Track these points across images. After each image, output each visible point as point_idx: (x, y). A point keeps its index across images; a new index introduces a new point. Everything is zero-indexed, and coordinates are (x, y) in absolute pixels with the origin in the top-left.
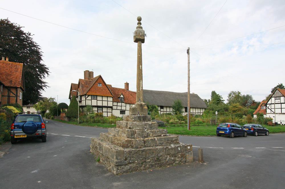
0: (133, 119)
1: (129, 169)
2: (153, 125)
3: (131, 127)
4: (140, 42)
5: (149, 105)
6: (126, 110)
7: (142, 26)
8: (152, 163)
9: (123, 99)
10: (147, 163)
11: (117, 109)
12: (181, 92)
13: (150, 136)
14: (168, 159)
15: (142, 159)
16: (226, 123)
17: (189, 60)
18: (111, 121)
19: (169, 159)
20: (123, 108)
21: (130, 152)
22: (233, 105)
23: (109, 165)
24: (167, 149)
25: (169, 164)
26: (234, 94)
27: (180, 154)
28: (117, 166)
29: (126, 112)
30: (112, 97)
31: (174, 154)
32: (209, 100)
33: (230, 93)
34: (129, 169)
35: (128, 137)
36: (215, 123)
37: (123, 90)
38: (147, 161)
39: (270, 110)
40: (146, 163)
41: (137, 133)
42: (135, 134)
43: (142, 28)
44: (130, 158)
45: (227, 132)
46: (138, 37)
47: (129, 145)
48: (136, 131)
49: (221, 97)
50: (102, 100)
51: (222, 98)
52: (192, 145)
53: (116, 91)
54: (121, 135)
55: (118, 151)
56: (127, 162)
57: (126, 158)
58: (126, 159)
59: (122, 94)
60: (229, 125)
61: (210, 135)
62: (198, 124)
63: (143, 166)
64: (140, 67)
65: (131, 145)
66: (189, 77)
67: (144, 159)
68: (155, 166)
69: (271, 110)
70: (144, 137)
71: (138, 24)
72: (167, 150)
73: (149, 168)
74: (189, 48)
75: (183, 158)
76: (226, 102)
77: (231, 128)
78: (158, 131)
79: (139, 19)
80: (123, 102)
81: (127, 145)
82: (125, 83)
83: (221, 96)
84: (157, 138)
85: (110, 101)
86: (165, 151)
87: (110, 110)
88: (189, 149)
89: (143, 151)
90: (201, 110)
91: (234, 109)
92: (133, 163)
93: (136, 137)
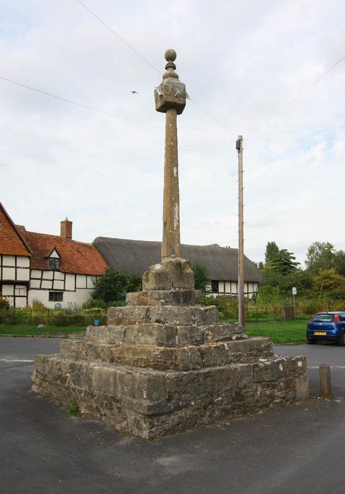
0: (160, 299)
1: (178, 424)
2: (208, 312)
3: (162, 319)
4: (174, 112)
5: (126, 276)
6: (64, 290)
7: (176, 71)
8: (226, 404)
9: (58, 263)
10: (215, 405)
11: (40, 289)
13: (207, 339)
14: (259, 393)
15: (204, 395)
16: (329, 313)
18: (36, 318)
19: (261, 393)
20: (58, 285)
21: (179, 380)
22: (322, 273)
23: (119, 418)
24: (257, 369)
25: (261, 407)
26: (320, 248)
27: (283, 379)
28: (150, 416)
29: (65, 294)
30: (29, 258)
31: (271, 381)
32: (261, 264)
33: (312, 247)
34: (178, 424)
35: (160, 345)
36: (292, 314)
37: (56, 239)
38: (216, 400)
40: (213, 406)
41: (179, 332)
42: (176, 335)
43: (176, 77)
44: (179, 395)
45: (332, 333)
46: (171, 99)
47: (169, 362)
48: (177, 329)
49: (292, 255)
50: (14, 266)
51: (294, 258)
52: (305, 358)
53: (37, 242)
54: (138, 340)
55: (153, 378)
56: (171, 405)
57: (169, 396)
58: (169, 400)
59: (55, 249)
60: (336, 316)
61: (293, 342)
62: (254, 319)
63: (208, 414)
64: (173, 172)
65: (172, 364)
66: (241, 206)
67: (209, 396)
68: (234, 413)
70: (196, 343)
71: (166, 68)
72: (257, 372)
73: (221, 418)
74: (240, 138)
75: (290, 391)
76: (304, 267)
77: (340, 322)
78: (224, 328)
79: (171, 57)
80: (59, 271)
81: (165, 362)
82: (61, 223)
83: (292, 254)
84: (228, 344)
85: (24, 268)
86: (253, 373)
87: (21, 291)
88: (301, 368)
89: (207, 375)
90: (250, 287)
91: (325, 282)
92: (187, 406)
93: (177, 343)
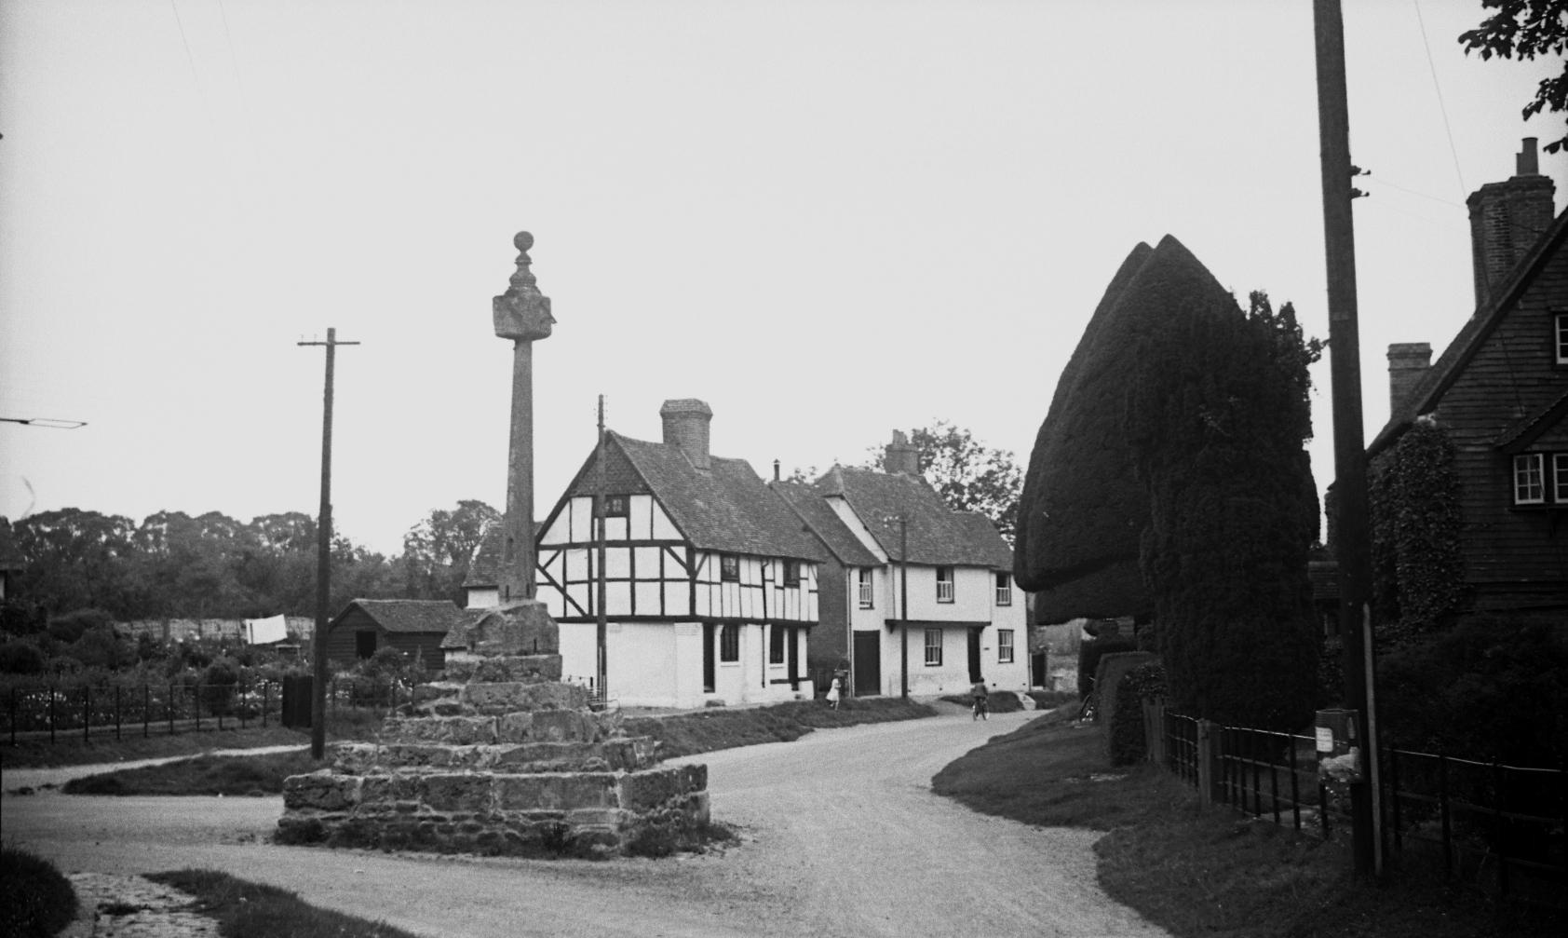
6: (741, 585)
12: (1043, 413)
17: (309, 344)
39: (560, 597)
69: (567, 598)
